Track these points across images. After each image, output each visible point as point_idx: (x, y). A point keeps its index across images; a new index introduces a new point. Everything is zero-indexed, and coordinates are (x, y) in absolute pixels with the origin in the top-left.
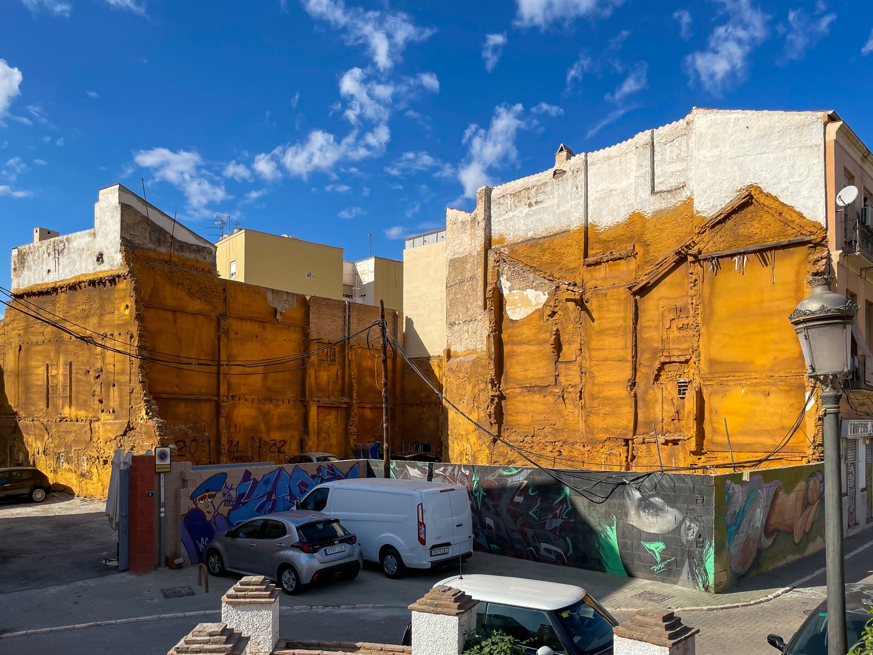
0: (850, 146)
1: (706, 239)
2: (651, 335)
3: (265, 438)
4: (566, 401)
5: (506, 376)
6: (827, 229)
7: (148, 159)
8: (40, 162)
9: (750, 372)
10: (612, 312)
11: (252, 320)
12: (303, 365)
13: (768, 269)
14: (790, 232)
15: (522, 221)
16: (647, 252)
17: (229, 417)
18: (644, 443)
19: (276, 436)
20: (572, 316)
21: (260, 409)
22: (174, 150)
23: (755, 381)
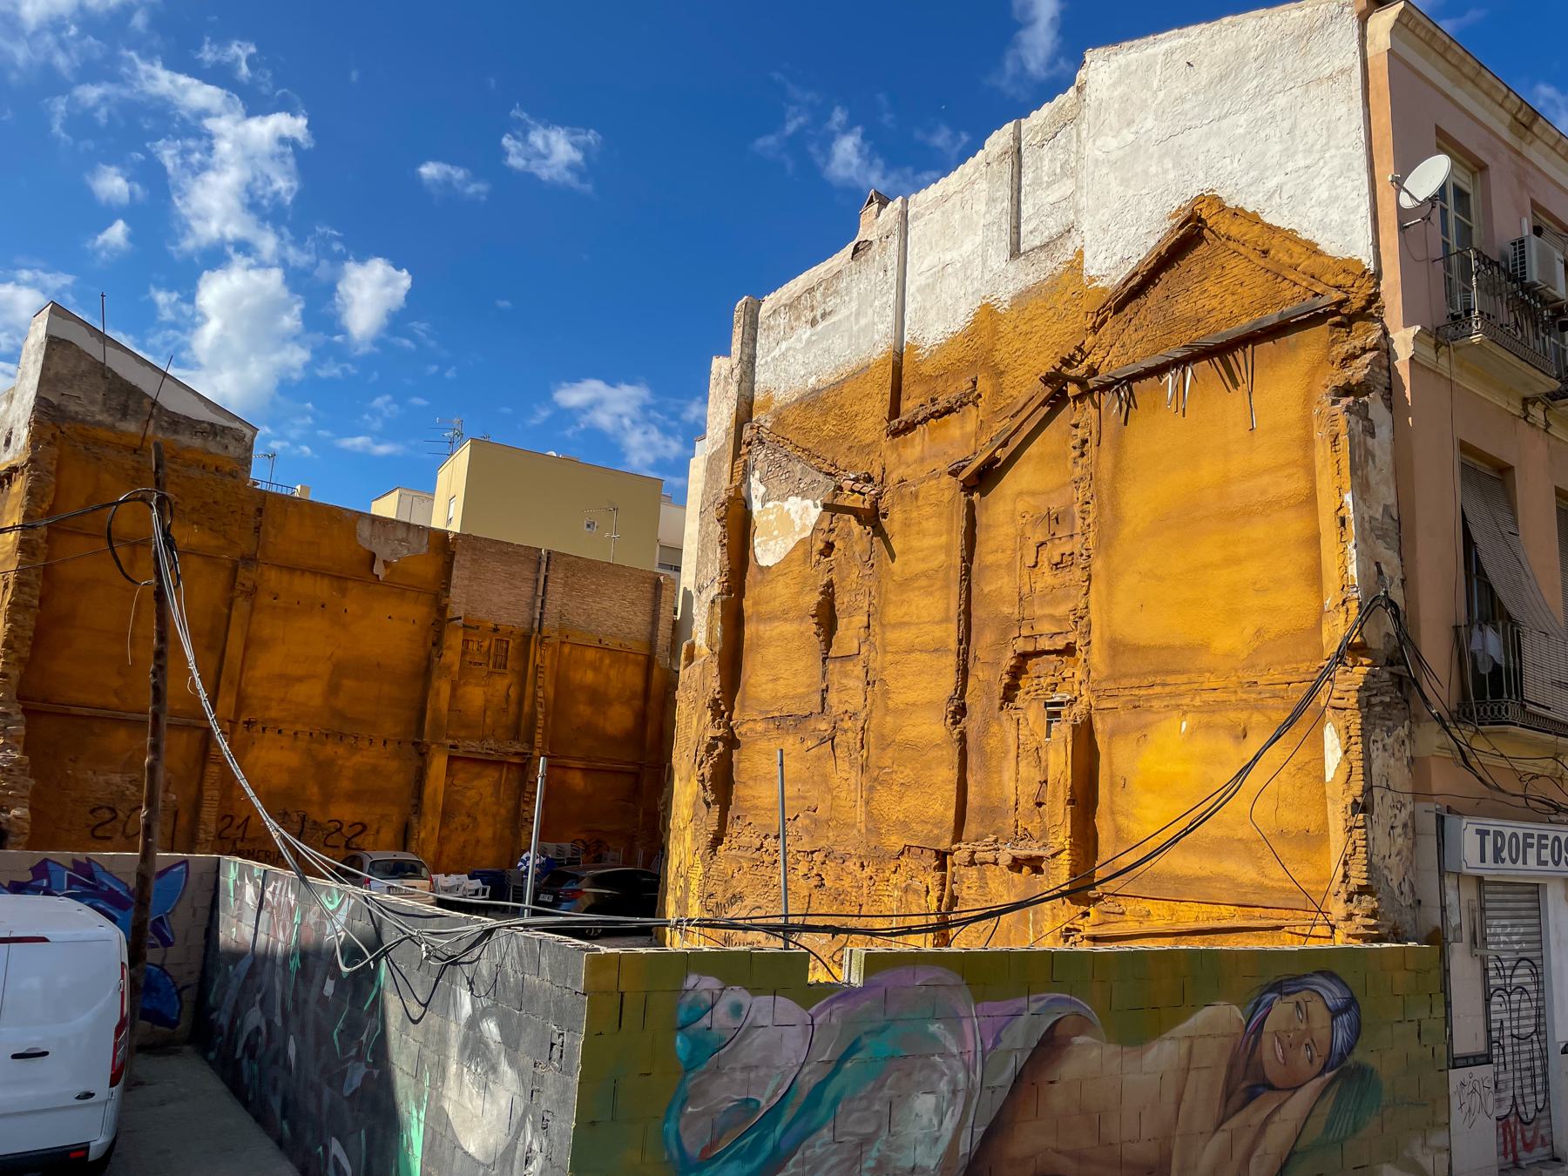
1: (1106, 340)
4: (838, 752)
5: (744, 693)
6: (1378, 275)
7: (573, 396)
8: (418, 401)
9: (1200, 672)
10: (925, 536)
11: (315, 572)
12: (425, 672)
13: (1238, 397)
14: (1288, 294)
15: (800, 357)
16: (998, 390)
18: (972, 863)
20: (857, 549)
22: (611, 382)
23: (1210, 697)
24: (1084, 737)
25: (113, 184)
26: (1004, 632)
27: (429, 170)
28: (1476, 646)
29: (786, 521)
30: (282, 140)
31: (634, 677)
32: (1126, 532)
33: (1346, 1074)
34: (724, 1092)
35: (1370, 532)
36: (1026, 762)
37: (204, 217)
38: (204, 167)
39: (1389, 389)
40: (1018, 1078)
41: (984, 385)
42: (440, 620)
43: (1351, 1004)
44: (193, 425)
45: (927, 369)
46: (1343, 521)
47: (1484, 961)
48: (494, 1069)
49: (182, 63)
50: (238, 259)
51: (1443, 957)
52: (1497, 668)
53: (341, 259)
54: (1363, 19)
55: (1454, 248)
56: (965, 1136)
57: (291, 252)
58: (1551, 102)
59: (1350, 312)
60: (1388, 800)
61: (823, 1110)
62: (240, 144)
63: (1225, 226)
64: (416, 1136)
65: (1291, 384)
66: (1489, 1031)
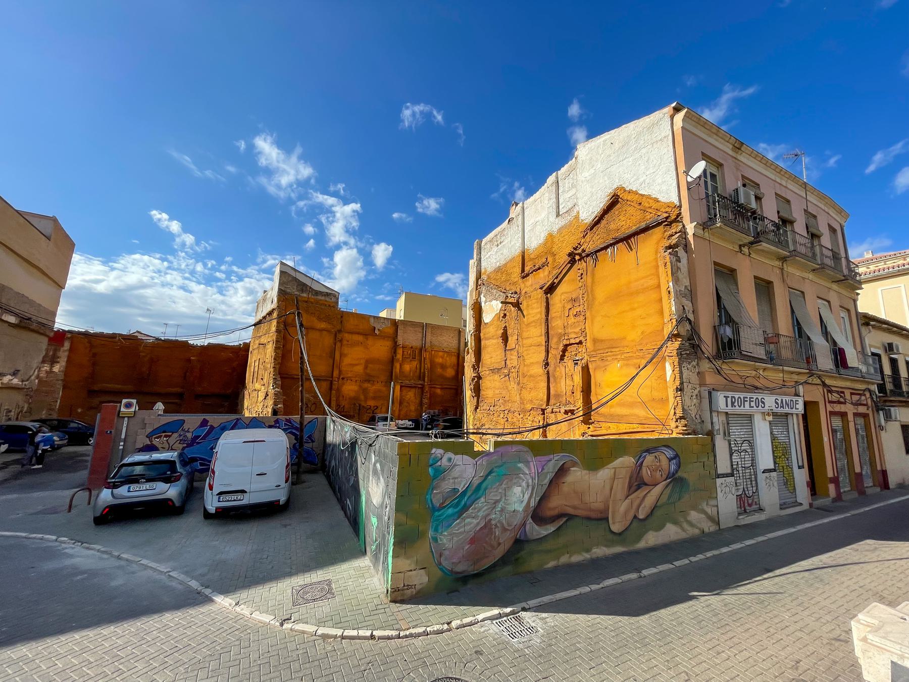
0: (710, 136)
1: (588, 240)
2: (557, 324)
3: (363, 404)
6: (680, 206)
7: (441, 278)
10: (534, 309)
11: (358, 333)
12: (392, 361)
16: (554, 260)
17: (339, 390)
19: (371, 403)
21: (360, 386)
22: (452, 273)
24: (586, 371)
25: (309, 229)
26: (560, 338)
27: (395, 215)
28: (722, 331)
29: (492, 309)
30: (354, 211)
31: (454, 360)
32: (597, 303)
33: (676, 480)
34: (446, 486)
35: (679, 295)
36: (568, 380)
37: (334, 236)
38: (333, 222)
39: (686, 246)
40: (551, 482)
41: (550, 259)
42: (395, 346)
43: (677, 456)
44: (321, 293)
45: (532, 256)
46: (669, 292)
47: (729, 442)
48: (379, 478)
49: (325, 192)
50: (345, 247)
51: (713, 440)
52: (730, 339)
53: (372, 244)
54: (672, 117)
55: (710, 193)
56: (533, 500)
57: (359, 244)
58: (765, 149)
59: (671, 220)
60: (690, 386)
61: (481, 492)
62: (342, 214)
63: (626, 196)
64: (363, 499)
65: (651, 248)
66: (732, 466)
